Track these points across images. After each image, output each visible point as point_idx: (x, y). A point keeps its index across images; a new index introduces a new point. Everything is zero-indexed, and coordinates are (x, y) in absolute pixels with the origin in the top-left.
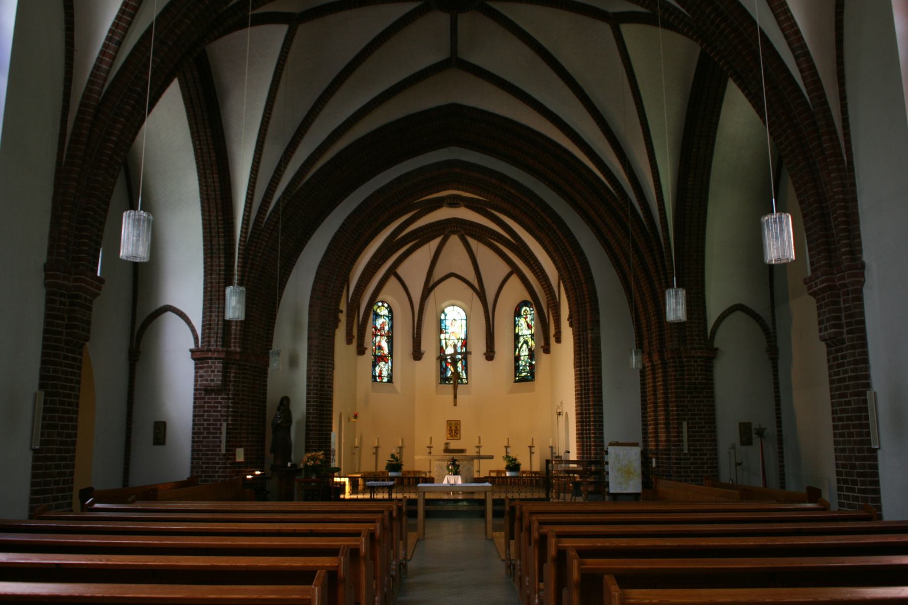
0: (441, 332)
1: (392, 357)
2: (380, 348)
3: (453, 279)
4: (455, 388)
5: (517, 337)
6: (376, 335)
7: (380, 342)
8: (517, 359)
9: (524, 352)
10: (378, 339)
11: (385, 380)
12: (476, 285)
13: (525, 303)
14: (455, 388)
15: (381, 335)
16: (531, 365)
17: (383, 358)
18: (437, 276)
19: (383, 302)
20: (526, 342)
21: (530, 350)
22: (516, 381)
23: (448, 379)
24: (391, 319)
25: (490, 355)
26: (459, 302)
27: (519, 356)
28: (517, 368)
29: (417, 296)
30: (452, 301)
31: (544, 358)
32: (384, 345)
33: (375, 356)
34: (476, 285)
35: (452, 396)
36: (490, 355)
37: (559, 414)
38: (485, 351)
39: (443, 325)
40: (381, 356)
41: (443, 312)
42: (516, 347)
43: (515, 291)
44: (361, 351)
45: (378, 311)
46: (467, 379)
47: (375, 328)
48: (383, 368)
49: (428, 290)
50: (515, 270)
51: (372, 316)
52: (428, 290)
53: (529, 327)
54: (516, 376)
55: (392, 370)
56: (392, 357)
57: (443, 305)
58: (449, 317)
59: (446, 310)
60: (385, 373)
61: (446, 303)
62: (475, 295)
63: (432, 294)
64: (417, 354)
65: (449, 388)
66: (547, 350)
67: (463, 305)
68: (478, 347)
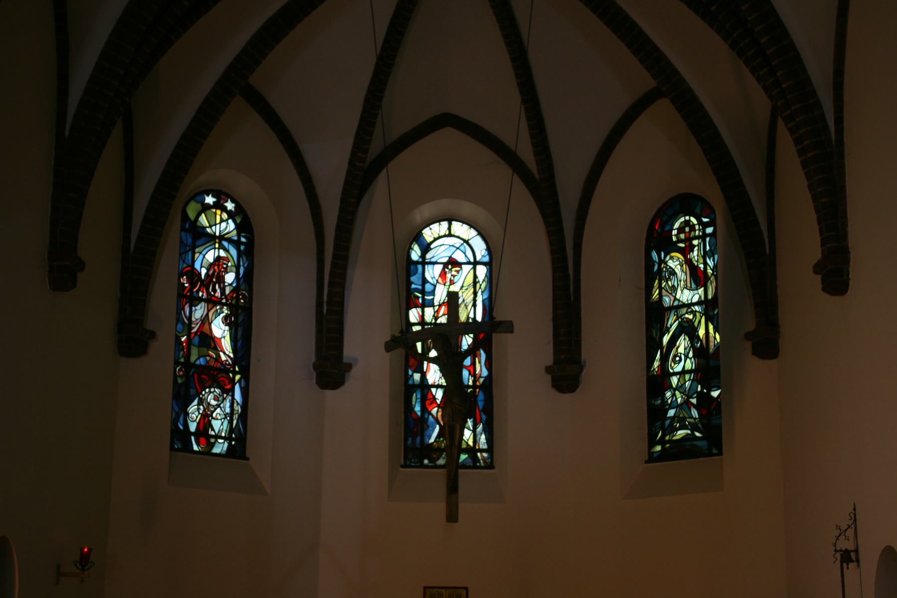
0: (411, 303)
1: (245, 374)
2: (209, 341)
3: (449, 134)
4: (453, 488)
5: (656, 315)
6: (194, 301)
7: (206, 321)
8: (658, 383)
9: (683, 361)
10: (199, 312)
11: (220, 447)
12: (526, 153)
13: (686, 203)
14: (453, 488)
15: (212, 302)
16: (705, 401)
17: (216, 376)
18: (398, 117)
19: (221, 196)
20: (688, 329)
21: (700, 352)
22: (652, 458)
23: (430, 451)
24: (247, 252)
25: (566, 373)
26: (467, 208)
27: (665, 374)
28: (656, 414)
29: (330, 164)
30: (444, 204)
31: (756, 373)
32: (219, 329)
33: (188, 365)
34: (526, 153)
35: (440, 508)
36: (566, 373)
37: (847, 557)
38: (549, 360)
39: (416, 279)
40: (206, 368)
41: (418, 237)
42: (653, 345)
43: (658, 156)
44: (133, 338)
45: (203, 220)
46: (490, 450)
47: (193, 275)
48: (217, 412)
49: (361, 177)
50: (669, 85)
51: (174, 234)
52: (361, 177)
53: (698, 278)
54: (652, 442)
55: (243, 417)
56: (245, 374)
57: (420, 214)
58: (440, 253)
59: (428, 234)
60: (219, 425)
61: (426, 210)
62: (520, 189)
63: (382, 177)
64: (331, 370)
65: (434, 480)
66: (766, 344)
67: (480, 214)
68: (531, 345)
